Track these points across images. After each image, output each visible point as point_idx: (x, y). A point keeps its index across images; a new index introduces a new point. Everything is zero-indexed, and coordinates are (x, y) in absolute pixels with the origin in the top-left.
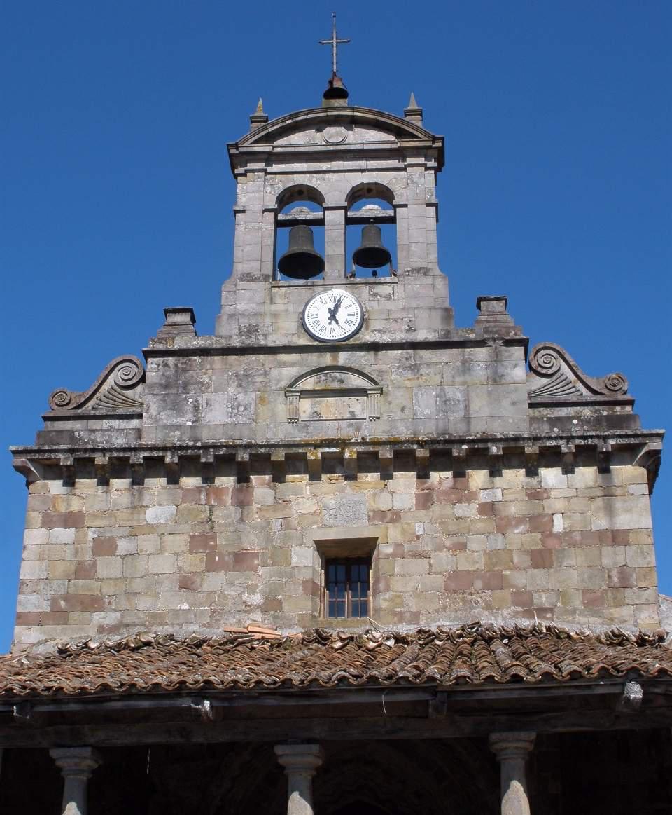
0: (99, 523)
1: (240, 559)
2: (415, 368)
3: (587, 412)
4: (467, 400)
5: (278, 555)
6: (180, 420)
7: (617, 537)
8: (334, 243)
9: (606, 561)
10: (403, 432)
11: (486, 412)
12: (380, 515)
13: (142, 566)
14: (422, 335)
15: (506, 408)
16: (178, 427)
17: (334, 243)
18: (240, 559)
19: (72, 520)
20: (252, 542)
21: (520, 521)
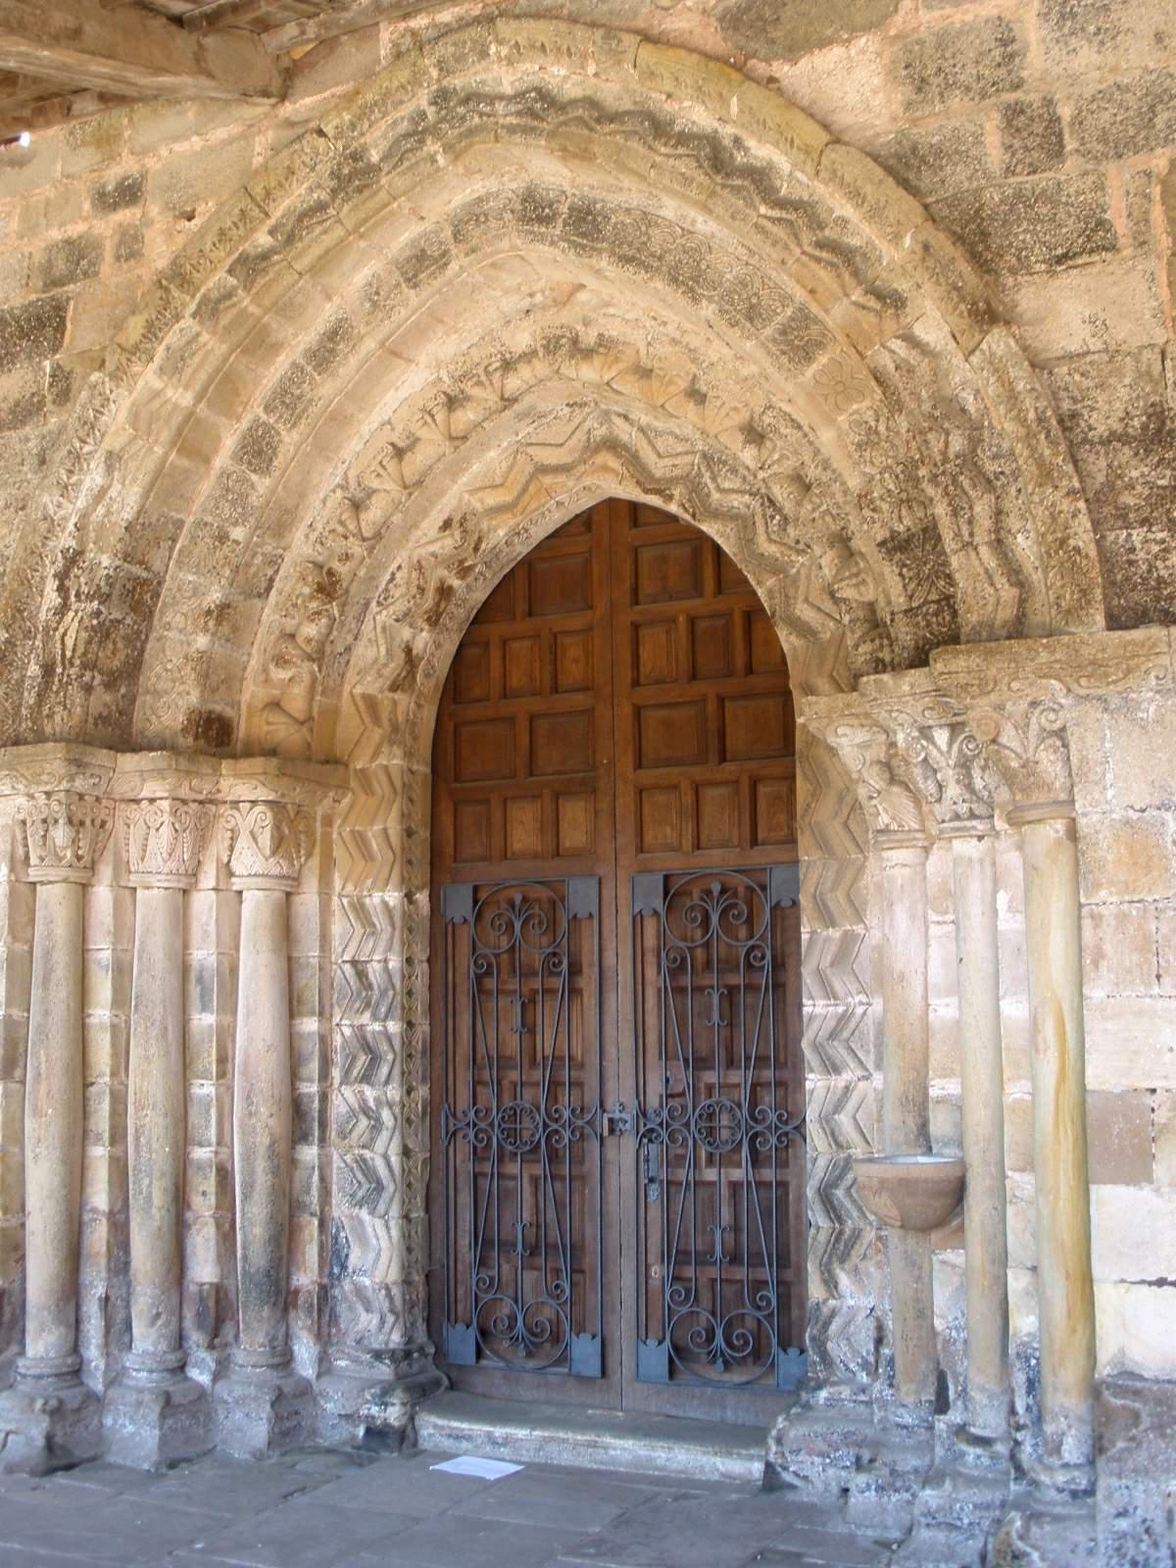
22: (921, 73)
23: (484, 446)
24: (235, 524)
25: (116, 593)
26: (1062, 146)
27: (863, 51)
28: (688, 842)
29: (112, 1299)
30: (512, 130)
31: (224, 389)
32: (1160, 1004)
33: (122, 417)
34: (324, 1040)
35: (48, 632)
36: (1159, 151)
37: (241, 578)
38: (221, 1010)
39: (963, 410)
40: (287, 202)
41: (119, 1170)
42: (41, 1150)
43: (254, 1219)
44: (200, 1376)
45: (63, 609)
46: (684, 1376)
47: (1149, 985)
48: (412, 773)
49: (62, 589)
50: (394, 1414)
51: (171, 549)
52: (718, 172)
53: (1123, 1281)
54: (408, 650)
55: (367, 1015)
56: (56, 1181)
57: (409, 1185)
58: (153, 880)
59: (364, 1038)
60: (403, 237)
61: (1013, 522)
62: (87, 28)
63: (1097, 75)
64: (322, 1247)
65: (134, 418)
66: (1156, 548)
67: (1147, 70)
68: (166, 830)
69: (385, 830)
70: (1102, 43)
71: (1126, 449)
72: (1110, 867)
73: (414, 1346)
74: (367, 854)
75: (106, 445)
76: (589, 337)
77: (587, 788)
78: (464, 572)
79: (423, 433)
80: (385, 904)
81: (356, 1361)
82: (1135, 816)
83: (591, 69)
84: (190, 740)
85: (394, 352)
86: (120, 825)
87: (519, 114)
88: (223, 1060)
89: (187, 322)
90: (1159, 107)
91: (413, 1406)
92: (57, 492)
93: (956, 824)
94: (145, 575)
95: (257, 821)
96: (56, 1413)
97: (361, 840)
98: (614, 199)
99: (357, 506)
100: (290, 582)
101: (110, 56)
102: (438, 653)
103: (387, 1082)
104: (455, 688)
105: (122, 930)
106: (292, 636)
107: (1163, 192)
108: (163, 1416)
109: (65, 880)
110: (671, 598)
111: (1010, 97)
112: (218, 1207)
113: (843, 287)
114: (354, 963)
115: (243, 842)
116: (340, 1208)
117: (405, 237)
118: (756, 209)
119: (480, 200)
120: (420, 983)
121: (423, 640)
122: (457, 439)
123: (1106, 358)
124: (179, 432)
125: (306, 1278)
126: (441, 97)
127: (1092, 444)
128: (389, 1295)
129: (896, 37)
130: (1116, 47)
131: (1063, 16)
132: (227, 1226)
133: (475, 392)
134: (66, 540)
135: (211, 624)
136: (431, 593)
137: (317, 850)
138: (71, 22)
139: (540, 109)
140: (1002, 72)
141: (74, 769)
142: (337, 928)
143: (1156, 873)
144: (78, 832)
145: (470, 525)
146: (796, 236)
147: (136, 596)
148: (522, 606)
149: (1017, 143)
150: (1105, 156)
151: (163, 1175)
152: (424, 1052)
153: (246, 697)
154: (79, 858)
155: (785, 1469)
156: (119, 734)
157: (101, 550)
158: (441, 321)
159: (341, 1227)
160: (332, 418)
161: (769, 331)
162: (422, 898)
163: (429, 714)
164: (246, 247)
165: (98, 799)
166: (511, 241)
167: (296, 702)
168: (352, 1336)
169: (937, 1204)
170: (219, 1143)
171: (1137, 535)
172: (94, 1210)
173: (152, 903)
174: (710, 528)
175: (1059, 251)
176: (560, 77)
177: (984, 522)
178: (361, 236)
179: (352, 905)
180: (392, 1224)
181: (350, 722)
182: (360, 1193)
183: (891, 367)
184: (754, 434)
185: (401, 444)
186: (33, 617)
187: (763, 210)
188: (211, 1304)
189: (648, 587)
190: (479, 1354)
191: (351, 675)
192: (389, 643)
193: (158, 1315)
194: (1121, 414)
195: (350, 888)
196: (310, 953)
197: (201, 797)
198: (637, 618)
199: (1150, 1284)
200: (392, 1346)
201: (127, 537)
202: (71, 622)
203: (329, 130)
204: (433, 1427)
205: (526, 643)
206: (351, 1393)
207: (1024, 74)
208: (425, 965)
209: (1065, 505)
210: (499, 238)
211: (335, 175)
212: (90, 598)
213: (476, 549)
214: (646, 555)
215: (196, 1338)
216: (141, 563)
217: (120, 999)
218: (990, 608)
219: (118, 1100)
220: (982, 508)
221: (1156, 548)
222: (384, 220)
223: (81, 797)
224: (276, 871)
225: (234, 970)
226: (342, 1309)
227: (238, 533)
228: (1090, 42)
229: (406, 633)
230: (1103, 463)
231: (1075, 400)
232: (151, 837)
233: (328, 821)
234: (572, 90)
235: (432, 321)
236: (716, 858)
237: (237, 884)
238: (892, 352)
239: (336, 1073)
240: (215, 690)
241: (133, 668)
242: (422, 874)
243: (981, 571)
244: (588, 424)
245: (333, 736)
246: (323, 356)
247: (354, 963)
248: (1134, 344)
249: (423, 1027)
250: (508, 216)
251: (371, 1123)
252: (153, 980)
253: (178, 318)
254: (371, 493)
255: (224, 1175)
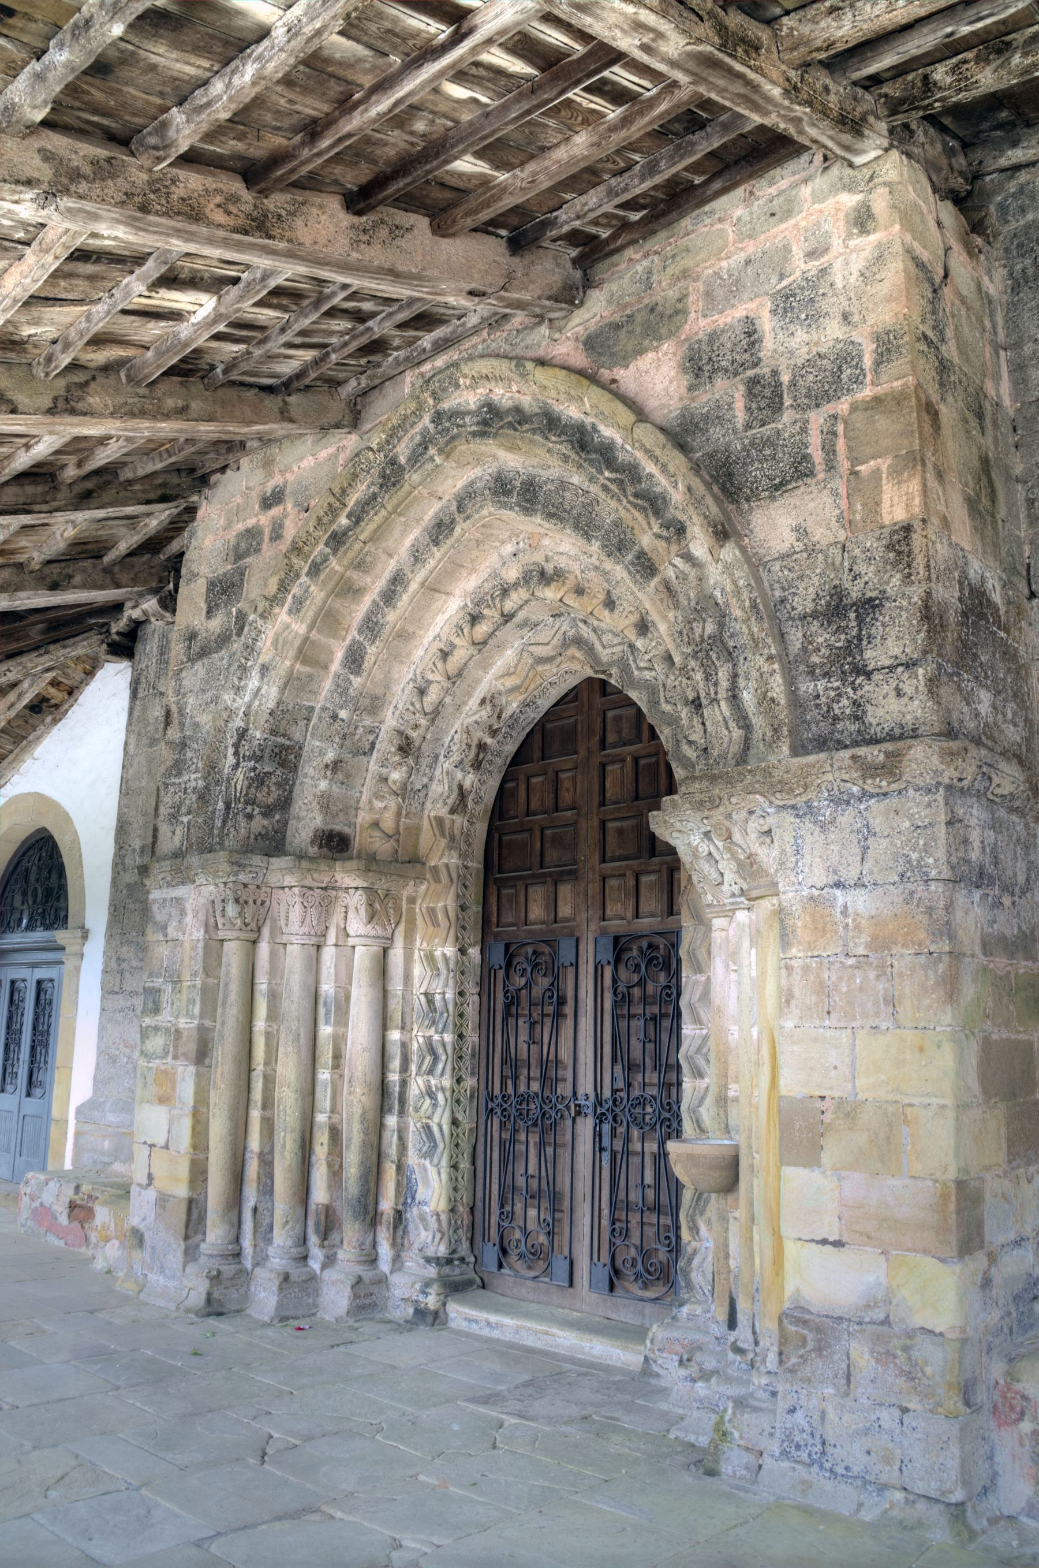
22: (699, 366)
23: (501, 647)
24: (341, 708)
25: (266, 755)
26: (782, 404)
27: (666, 354)
28: (629, 915)
29: (260, 1209)
30: (474, 434)
31: (328, 620)
32: (830, 1033)
33: (268, 643)
34: (404, 1046)
35: (229, 780)
36: (843, 399)
37: (348, 742)
38: (337, 1023)
39: (717, 604)
40: (356, 496)
41: (268, 1126)
42: (216, 1110)
43: (352, 1160)
44: (315, 1265)
45: (237, 766)
46: (619, 1291)
47: (822, 1019)
48: (467, 868)
49: (236, 754)
50: (432, 1301)
51: (307, 725)
52: (583, 450)
53: (800, 1239)
54: (460, 787)
55: (433, 1029)
56: (225, 1131)
57: (457, 1145)
58: (293, 939)
59: (431, 1045)
60: (431, 511)
61: (742, 683)
62: (193, 405)
63: (805, 349)
64: (398, 1184)
65: (275, 642)
66: (832, 694)
67: (837, 340)
68: (298, 907)
69: (445, 907)
70: (810, 325)
71: (815, 622)
72: (799, 931)
73: (456, 1256)
74: (436, 924)
75: (260, 661)
76: (549, 568)
77: (572, 875)
78: (493, 732)
79: (457, 641)
80: (444, 955)
81: (417, 1263)
82: (815, 892)
83: (515, 388)
84: (316, 848)
85: (433, 589)
86: (274, 903)
87: (478, 424)
88: (337, 1056)
89: (303, 579)
90: (844, 366)
91: (446, 1296)
92: (232, 692)
93: (732, 900)
94: (288, 743)
95: (357, 900)
96: (216, 1278)
97: (432, 912)
98: (545, 474)
99: (422, 692)
100: (386, 744)
101: (210, 419)
102: (483, 788)
103: (442, 1075)
104: (499, 810)
105: (275, 970)
106: (386, 779)
107: (845, 428)
108: (280, 1289)
109: (237, 939)
110: (624, 745)
111: (750, 373)
112: (329, 1154)
113: (649, 523)
114: (426, 994)
115: (351, 915)
116: (413, 1159)
117: (431, 513)
118: (602, 473)
119: (472, 483)
120: (471, 1011)
121: (470, 780)
122: (480, 645)
123: (805, 555)
124: (300, 651)
125: (387, 1205)
126: (438, 417)
127: (793, 619)
128: (439, 1220)
129: (686, 340)
130: (818, 328)
131: (785, 311)
132: (337, 1167)
133: (486, 612)
134: (238, 722)
135: (329, 773)
136: (474, 750)
137: (403, 919)
138: (180, 403)
139: (492, 420)
140: (747, 356)
141: (236, 868)
142: (417, 970)
143: (828, 935)
144: (243, 908)
145: (496, 701)
146: (624, 490)
147: (285, 757)
148: (537, 754)
149: (754, 406)
150: (809, 407)
151: (293, 1131)
152: (473, 1056)
153: (359, 820)
154: (246, 925)
155: (655, 1362)
156: (273, 844)
157: (256, 728)
158: (462, 566)
159: (413, 1172)
160: (399, 636)
161: (630, 557)
162: (474, 952)
163: (481, 829)
164: (335, 527)
165: (258, 887)
166: (489, 510)
167: (388, 823)
168: (416, 1246)
169: (716, 1174)
170: (332, 1111)
171: (821, 685)
172: (252, 1152)
173: (295, 956)
174: (633, 695)
175: (777, 481)
176: (503, 395)
177: (724, 684)
178: (400, 515)
179: (426, 956)
180: (442, 1171)
181: (427, 835)
182: (425, 1149)
183: (674, 576)
185: (446, 649)
186: (220, 772)
187: (607, 474)
188: (323, 1217)
189: (611, 738)
190: (500, 1266)
191: (429, 805)
192: (450, 782)
193: (287, 1222)
194: (813, 596)
195: (425, 945)
196: (396, 986)
197: (324, 885)
198: (604, 760)
199: (818, 1242)
200: (439, 1254)
201: (271, 720)
202: (240, 774)
203: (374, 446)
204: (458, 1313)
205: (540, 779)
206: (409, 1282)
207: (761, 355)
208: (476, 997)
209: (766, 668)
210: (481, 507)
211: (383, 476)
212: (250, 759)
213: (499, 717)
214: (610, 714)
215: (313, 1239)
216: (284, 735)
217: (273, 1015)
218: (725, 745)
219: (269, 1080)
220: (723, 675)
221: (832, 694)
222: (411, 504)
223: (245, 885)
224: (373, 933)
225: (348, 998)
226: (411, 1227)
227: (343, 714)
228: (801, 325)
229: (459, 775)
230: (800, 635)
231: (783, 589)
232: (292, 913)
233: (412, 900)
234: (506, 403)
235: (453, 569)
236: (645, 924)
237: (351, 941)
238: (675, 566)
239: (413, 1068)
240: (335, 816)
241: (285, 804)
242: (473, 935)
243: (720, 718)
244: (563, 629)
245: (416, 844)
246: (389, 597)
247: (426, 994)
248: (824, 542)
249: (472, 1038)
250: (487, 492)
251: (432, 1102)
252: (294, 1002)
253: (298, 576)
254: (429, 682)
255: (335, 1133)
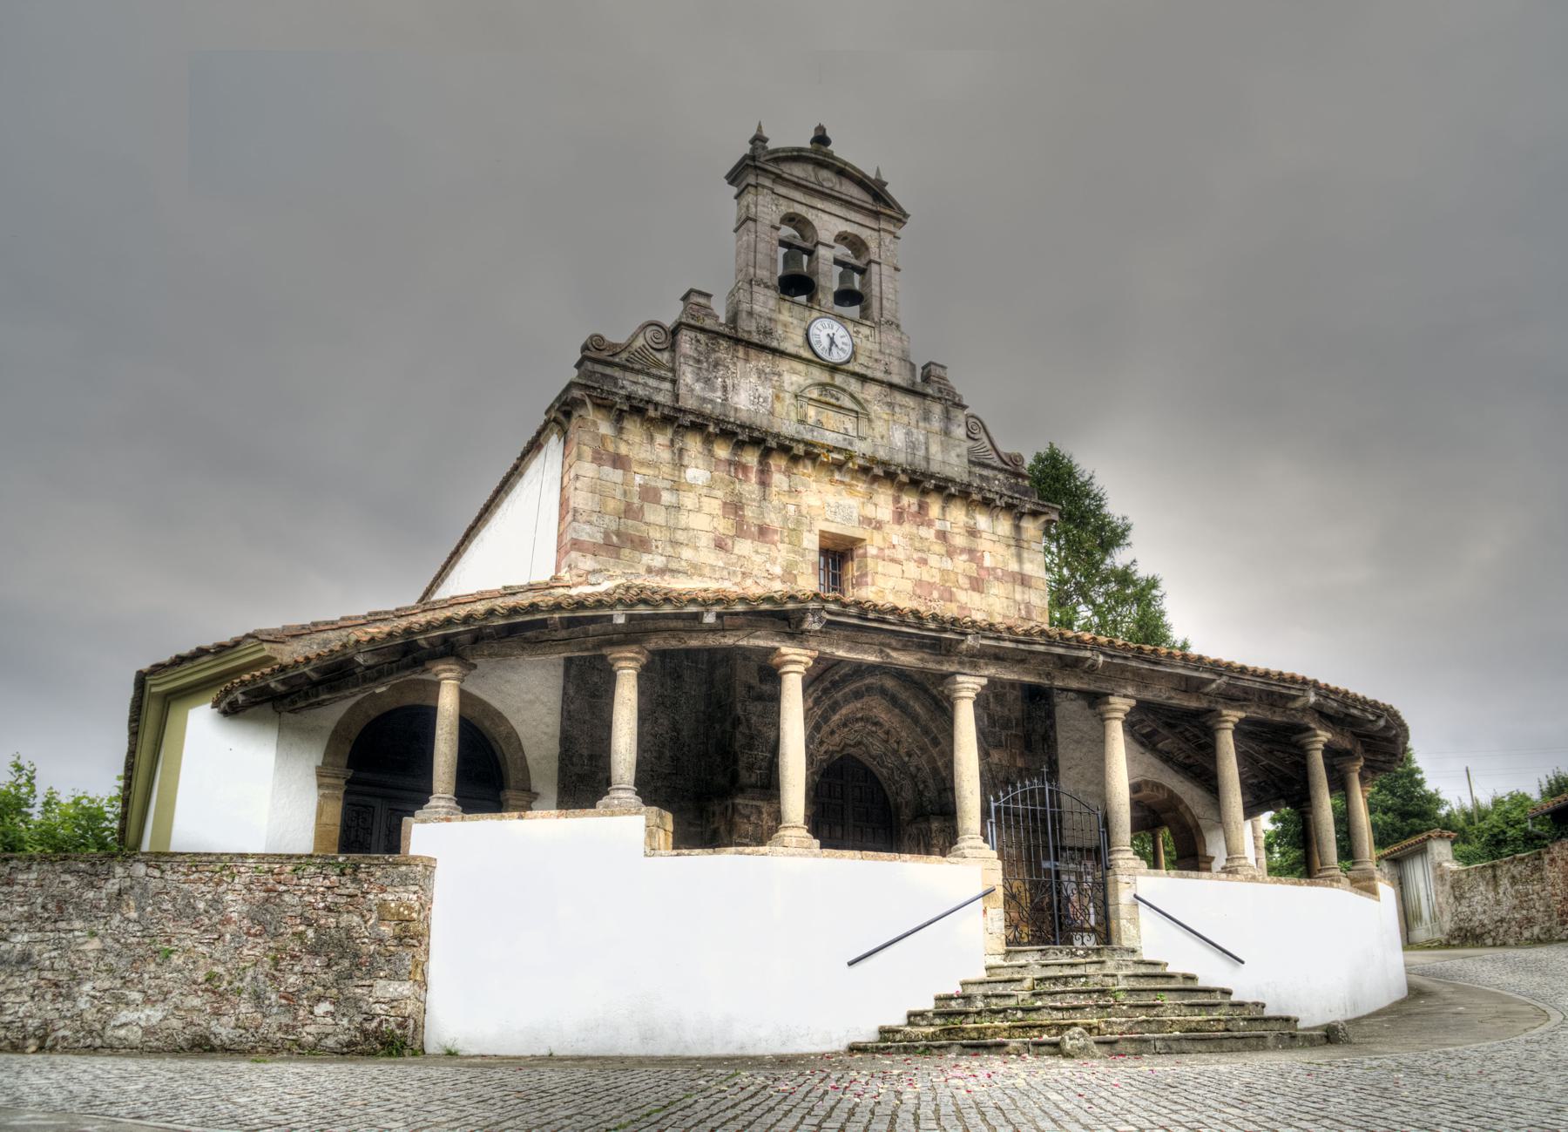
0: (644, 471)
1: (763, 532)
2: (891, 405)
3: (1000, 476)
4: (927, 443)
5: (795, 532)
6: (709, 395)
7: (1024, 581)
8: (830, 280)
9: (1018, 597)
10: (882, 454)
11: (939, 457)
12: (867, 521)
13: (684, 519)
14: (896, 379)
15: (953, 459)
16: (711, 401)
17: (830, 280)
18: (763, 532)
19: (619, 462)
20: (773, 520)
21: (963, 551)
184: (909, 755)
